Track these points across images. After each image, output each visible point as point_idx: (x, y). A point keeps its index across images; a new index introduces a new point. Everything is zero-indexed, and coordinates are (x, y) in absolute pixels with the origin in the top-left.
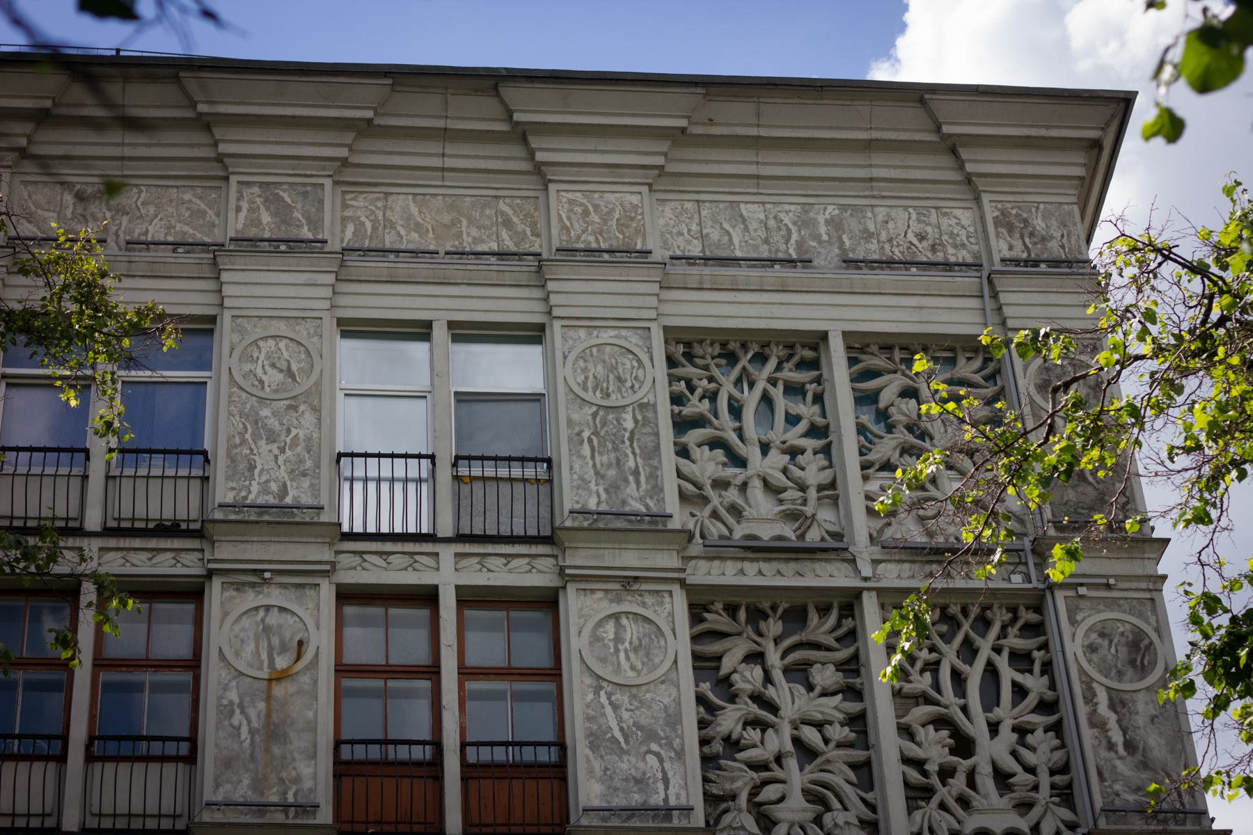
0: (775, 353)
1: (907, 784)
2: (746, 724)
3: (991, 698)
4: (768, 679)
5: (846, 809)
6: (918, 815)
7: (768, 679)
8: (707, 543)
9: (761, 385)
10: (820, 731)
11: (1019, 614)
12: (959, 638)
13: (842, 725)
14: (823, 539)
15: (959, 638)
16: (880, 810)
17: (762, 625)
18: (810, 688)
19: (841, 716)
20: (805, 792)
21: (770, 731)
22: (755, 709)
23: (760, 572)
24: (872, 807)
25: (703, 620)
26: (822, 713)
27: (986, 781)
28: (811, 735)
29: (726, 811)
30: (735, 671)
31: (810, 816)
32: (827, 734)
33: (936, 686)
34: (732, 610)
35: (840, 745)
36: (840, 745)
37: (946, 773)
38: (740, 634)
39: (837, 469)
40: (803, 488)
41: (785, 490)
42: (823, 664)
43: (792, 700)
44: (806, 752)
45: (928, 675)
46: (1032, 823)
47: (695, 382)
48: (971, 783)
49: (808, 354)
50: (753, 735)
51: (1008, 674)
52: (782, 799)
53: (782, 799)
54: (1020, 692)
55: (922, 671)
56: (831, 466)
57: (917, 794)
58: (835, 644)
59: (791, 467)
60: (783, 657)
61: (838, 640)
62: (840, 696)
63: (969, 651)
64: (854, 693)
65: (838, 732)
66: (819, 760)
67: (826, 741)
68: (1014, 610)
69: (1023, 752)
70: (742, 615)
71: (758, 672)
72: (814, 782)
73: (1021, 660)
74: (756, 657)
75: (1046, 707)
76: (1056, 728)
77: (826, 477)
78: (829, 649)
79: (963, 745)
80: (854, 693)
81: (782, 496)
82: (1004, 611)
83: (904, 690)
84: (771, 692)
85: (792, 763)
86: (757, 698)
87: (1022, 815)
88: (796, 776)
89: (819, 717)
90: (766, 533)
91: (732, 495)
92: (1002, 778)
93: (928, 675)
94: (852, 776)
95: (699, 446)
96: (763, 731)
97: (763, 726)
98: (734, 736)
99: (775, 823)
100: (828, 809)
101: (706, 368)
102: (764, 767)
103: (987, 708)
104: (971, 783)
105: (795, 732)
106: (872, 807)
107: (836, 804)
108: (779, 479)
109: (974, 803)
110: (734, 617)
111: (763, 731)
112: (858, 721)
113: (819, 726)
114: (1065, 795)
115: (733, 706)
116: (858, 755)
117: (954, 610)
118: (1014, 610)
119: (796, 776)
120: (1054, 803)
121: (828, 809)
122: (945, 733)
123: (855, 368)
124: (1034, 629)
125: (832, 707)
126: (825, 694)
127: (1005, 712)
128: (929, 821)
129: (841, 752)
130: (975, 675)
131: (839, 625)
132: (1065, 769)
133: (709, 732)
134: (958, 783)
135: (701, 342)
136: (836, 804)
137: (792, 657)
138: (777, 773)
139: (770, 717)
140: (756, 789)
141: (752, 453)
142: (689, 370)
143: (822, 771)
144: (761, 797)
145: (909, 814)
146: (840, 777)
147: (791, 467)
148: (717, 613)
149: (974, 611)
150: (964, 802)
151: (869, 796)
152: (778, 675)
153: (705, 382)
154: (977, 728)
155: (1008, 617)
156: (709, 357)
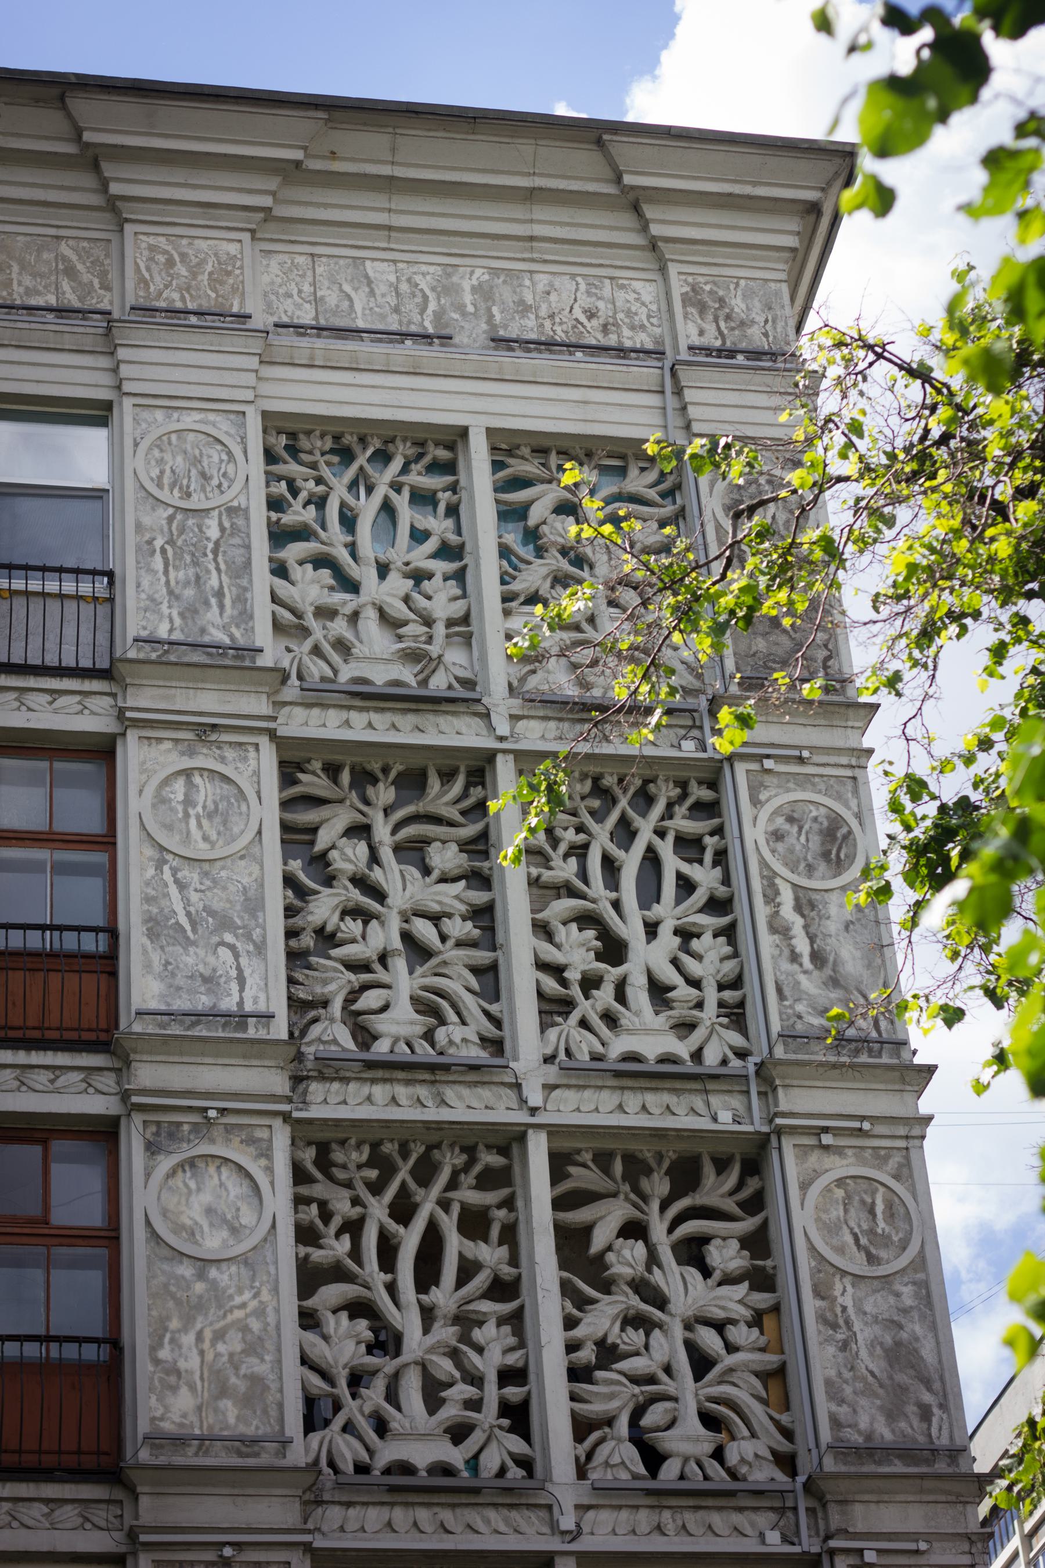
0: (401, 452)
1: (540, 995)
3: (649, 893)
4: (374, 859)
6: (552, 1034)
7: (374, 859)
9: (382, 490)
10: (436, 926)
13: (750, 1325)
14: (450, 687)
15: (614, 817)
16: (506, 1025)
18: (426, 871)
19: (463, 908)
20: (415, 1000)
21: (657, 1333)
22: (356, 895)
23: (370, 725)
24: (497, 1023)
30: (609, 1248)
31: (420, 1030)
32: (445, 930)
34: (332, 771)
36: (459, 944)
39: (472, 599)
41: (405, 623)
44: (418, 951)
48: (621, 996)
49: (443, 454)
52: (385, 1008)
55: (566, 856)
56: (464, 596)
57: (554, 1008)
59: (416, 596)
61: (463, 813)
63: (403, 1211)
64: (481, 880)
65: (458, 928)
66: (434, 961)
67: (443, 938)
69: (686, 959)
73: (689, 846)
74: (360, 831)
75: (717, 905)
76: (729, 933)
77: (457, 609)
78: (451, 824)
80: (762, 1280)
81: (402, 631)
82: (671, 785)
83: (543, 879)
84: (657, 1277)
85: (400, 964)
86: (360, 882)
87: (682, 1038)
88: (404, 980)
89: (720, 1314)
90: (380, 676)
91: (339, 627)
93: (573, 861)
95: (301, 563)
96: (366, 923)
97: (365, 916)
98: (329, 928)
99: (375, 1038)
100: (443, 1022)
101: (314, 466)
102: (364, 967)
103: (644, 905)
104: (392, 1396)
105: (406, 926)
106: (497, 1023)
107: (451, 1016)
108: (400, 610)
109: (394, 1425)
111: (366, 923)
112: (484, 916)
114: (736, 1015)
115: (328, 891)
116: (482, 956)
117: (609, 781)
119: (404, 980)
120: (721, 1025)
121: (443, 1022)
124: (709, 809)
125: (453, 896)
126: (443, 880)
128: (567, 1041)
129: (462, 952)
131: (465, 795)
132: (736, 983)
133: (578, 1332)
136: (451, 1016)
138: (668, 1386)
140: (354, 995)
141: (367, 575)
143: (436, 975)
146: (459, 983)
151: (494, 1008)
153: (311, 484)
154: (631, 930)
156: (318, 453)
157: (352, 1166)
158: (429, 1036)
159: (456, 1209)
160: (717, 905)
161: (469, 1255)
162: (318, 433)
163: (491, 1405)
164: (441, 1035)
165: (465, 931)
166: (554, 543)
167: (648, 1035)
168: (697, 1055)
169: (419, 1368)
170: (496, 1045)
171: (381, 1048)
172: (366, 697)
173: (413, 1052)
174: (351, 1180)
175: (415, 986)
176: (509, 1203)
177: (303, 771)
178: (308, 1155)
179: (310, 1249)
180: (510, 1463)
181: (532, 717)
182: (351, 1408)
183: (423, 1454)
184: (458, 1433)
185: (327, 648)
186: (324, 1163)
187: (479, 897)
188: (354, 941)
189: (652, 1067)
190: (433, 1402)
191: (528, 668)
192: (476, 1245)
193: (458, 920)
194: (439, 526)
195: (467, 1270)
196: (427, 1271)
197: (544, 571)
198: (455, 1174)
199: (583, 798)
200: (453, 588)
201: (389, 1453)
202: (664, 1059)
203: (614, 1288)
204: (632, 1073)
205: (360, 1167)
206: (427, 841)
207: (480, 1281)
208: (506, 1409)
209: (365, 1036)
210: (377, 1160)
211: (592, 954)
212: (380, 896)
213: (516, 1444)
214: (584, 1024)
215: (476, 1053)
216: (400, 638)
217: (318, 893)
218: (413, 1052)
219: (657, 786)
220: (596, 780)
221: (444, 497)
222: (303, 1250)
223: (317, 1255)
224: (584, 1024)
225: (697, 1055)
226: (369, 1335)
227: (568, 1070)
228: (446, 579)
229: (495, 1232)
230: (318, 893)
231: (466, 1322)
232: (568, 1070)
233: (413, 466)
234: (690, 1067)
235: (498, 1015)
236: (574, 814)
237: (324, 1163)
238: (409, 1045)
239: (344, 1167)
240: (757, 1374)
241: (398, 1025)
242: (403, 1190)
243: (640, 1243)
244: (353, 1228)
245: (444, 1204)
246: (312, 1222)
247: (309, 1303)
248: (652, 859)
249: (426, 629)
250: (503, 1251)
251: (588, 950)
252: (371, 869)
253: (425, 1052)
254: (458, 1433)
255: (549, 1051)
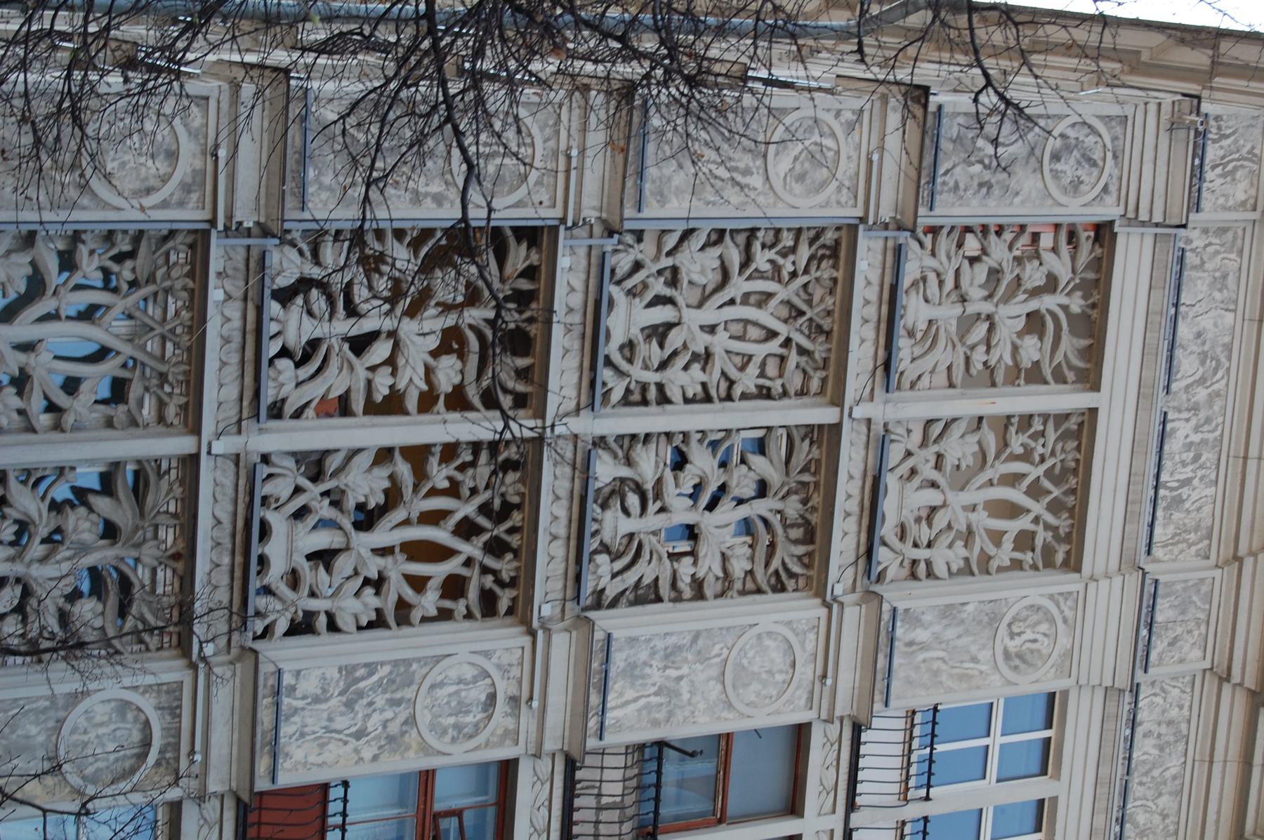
0: (1063, 523)
1: (327, 453)
2: (397, 282)
3: (416, 551)
4: (447, 308)
5: (298, 385)
6: (290, 463)
7: (740, 502)
8: (607, 255)
9: (783, 329)
11: (507, 591)
12: (483, 521)
13: (391, 387)
14: (879, 563)
15: (483, 521)
16: (294, 423)
17: (794, 498)
18: (435, 354)
19: (401, 385)
20: (631, 536)
21: (691, 503)
22: (712, 488)
23: (849, 496)
24: (298, 414)
25: (519, 241)
26: (706, 555)
27: (323, 540)
28: (381, 350)
29: (301, 253)
31: (607, 540)
33: (433, 492)
34: (530, 273)
35: (369, 382)
37: (336, 499)
38: (787, 474)
39: (948, 582)
40: (663, 365)
41: (930, 525)
42: (462, 372)
43: (419, 336)
44: (360, 344)
45: (446, 484)
46: (273, 587)
47: (791, 258)
49: (1060, 557)
50: (382, 285)
51: (438, 571)
53: (626, 512)
54: (996, 537)
55: (450, 479)
56: (950, 573)
57: (315, 465)
58: (772, 569)
59: (952, 534)
60: (471, 327)
61: (777, 572)
62: (425, 387)
63: (467, 529)
64: (427, 402)
67: (373, 369)
68: (513, 583)
70: (524, 285)
71: (749, 490)
72: (640, 546)
73: (454, 587)
74: (763, 489)
77: (674, 393)
78: (767, 565)
79: (367, 519)
81: (924, 523)
82: (513, 574)
83: (81, 246)
89: (401, 361)
90: (889, 506)
91: (928, 472)
92: (324, 557)
93: (446, 484)
94: (334, 394)
95: (979, 443)
96: (691, 496)
97: (394, 298)
100: (298, 365)
101: (1053, 454)
102: (658, 495)
104: (323, 524)
106: (298, 414)
108: (940, 520)
109: (300, 525)
110: (805, 469)
111: (691, 496)
112: (393, 405)
113: (391, 362)
114: (302, 627)
115: (716, 463)
116: (358, 403)
117: (516, 518)
118: (513, 583)
121: (298, 365)
122: (381, 499)
123: (509, 233)
124: (488, 605)
125: (411, 378)
127: (397, 568)
128: (279, 475)
129: (362, 384)
130: (440, 535)
132: (333, 627)
134: (324, 510)
135: (1078, 448)
137: (471, 337)
138: (652, 507)
139: (705, 499)
141: (709, 314)
142: (804, 252)
144: (314, 293)
145: (293, 454)
146: (335, 381)
147: (952, 534)
148: (809, 452)
149: (514, 540)
150: (301, 514)
151: (310, 412)
152: (744, 511)
153: (1040, 450)
154: (383, 535)
155: (505, 577)
156: (1063, 456)
157: (503, 489)
158: (284, 352)
159: (464, 572)
160: (403, 608)
161: (430, 584)
162: (1078, 456)
163: (313, 605)
164: (285, 364)
165: (380, 387)
166: (731, 477)
167: (286, 546)
168: (267, 591)
169: (343, 546)
170: (276, 411)
171: (593, 509)
172: (597, 308)
173: (271, 338)
174: (154, 282)
175: (642, 536)
176: (469, 616)
177: (529, 248)
178: (512, 453)
179: (438, 456)
180: (267, 621)
181: (575, 454)
182: (315, 490)
183: (275, 550)
184: (294, 579)
185: (910, 463)
186: (509, 466)
187: (412, 402)
188: (677, 486)
189: (256, 550)
190: (315, 556)
191: (305, 248)
192: (436, 589)
193: (390, 381)
194: (748, 381)
195: (418, 583)
196: (416, 551)
197: (708, 471)
198: (494, 572)
199: (503, 495)
200: (694, 390)
201: (278, 521)
202: (263, 561)
203: (54, 513)
204: (249, 533)
205: (503, 495)
206: (462, 356)
207: (409, 594)
208: (310, 615)
209: (285, 296)
210: (508, 508)
211: (362, 499)
212: (711, 507)
213: (282, 625)
214: (298, 490)
215: (269, 394)
216: (918, 520)
217: (714, 456)
218: (271, 338)
219: (510, 561)
220: (518, 507)
221: (1028, 557)
222: (438, 449)
223: (434, 461)
224: (298, 490)
225: (267, 591)
226: (372, 505)
227: (250, 474)
228: (704, 385)
229: (447, 604)
230: (714, 456)
231: (378, 584)
232: (250, 474)
233: (1050, 534)
234: (255, 583)
235: (304, 416)
236: (487, 487)
237: (509, 466)
238: (278, 334)
239: (503, 482)
240: (348, 392)
241: (614, 524)
242: (479, 530)
243: (753, 494)
244: (453, 490)
245: (468, 562)
246: (458, 456)
247: (397, 456)
248: (440, 553)
249: (925, 543)
250: (433, 612)
251: (366, 496)
252: (733, 499)
253: (591, 544)
254: (294, 579)
255: (274, 458)
